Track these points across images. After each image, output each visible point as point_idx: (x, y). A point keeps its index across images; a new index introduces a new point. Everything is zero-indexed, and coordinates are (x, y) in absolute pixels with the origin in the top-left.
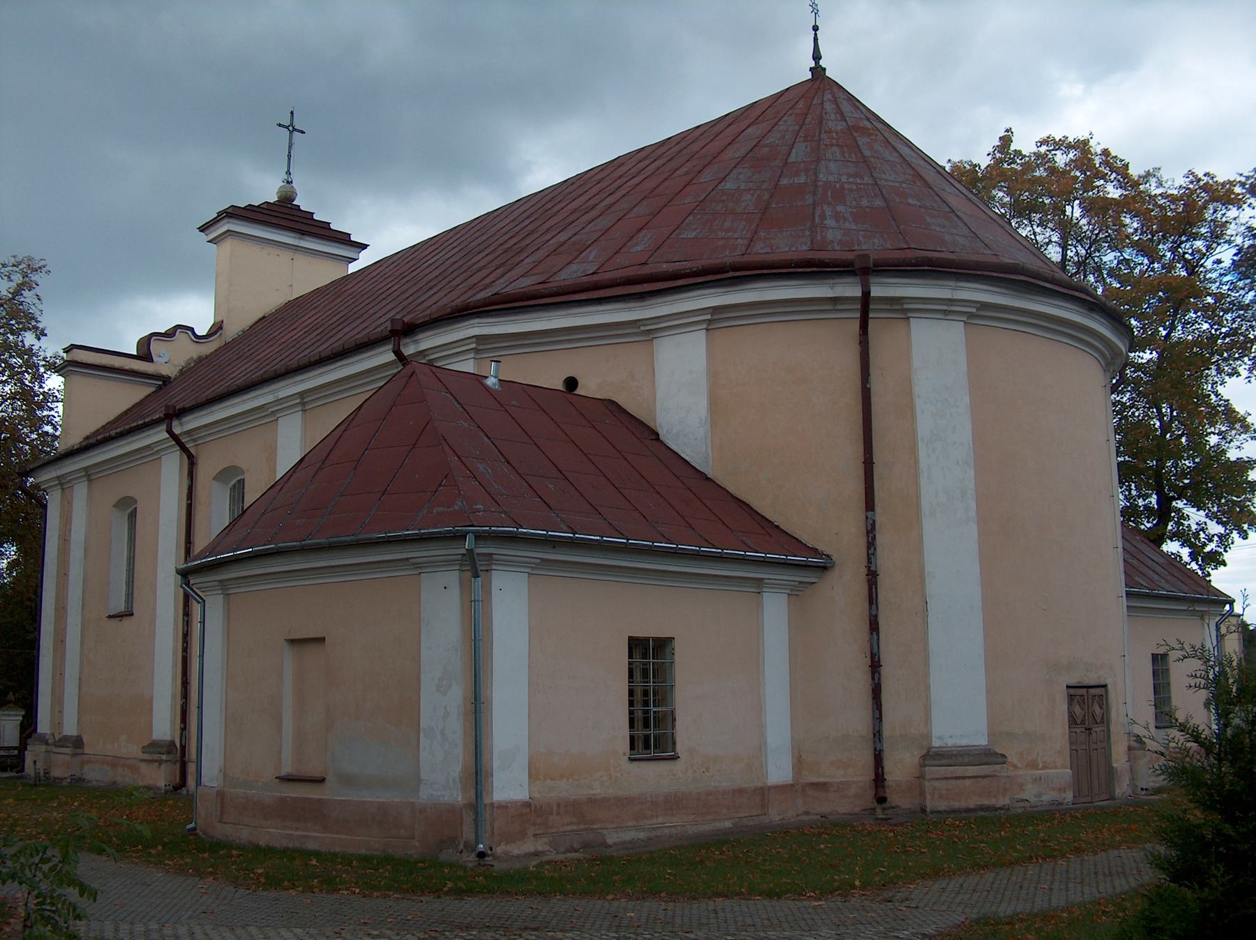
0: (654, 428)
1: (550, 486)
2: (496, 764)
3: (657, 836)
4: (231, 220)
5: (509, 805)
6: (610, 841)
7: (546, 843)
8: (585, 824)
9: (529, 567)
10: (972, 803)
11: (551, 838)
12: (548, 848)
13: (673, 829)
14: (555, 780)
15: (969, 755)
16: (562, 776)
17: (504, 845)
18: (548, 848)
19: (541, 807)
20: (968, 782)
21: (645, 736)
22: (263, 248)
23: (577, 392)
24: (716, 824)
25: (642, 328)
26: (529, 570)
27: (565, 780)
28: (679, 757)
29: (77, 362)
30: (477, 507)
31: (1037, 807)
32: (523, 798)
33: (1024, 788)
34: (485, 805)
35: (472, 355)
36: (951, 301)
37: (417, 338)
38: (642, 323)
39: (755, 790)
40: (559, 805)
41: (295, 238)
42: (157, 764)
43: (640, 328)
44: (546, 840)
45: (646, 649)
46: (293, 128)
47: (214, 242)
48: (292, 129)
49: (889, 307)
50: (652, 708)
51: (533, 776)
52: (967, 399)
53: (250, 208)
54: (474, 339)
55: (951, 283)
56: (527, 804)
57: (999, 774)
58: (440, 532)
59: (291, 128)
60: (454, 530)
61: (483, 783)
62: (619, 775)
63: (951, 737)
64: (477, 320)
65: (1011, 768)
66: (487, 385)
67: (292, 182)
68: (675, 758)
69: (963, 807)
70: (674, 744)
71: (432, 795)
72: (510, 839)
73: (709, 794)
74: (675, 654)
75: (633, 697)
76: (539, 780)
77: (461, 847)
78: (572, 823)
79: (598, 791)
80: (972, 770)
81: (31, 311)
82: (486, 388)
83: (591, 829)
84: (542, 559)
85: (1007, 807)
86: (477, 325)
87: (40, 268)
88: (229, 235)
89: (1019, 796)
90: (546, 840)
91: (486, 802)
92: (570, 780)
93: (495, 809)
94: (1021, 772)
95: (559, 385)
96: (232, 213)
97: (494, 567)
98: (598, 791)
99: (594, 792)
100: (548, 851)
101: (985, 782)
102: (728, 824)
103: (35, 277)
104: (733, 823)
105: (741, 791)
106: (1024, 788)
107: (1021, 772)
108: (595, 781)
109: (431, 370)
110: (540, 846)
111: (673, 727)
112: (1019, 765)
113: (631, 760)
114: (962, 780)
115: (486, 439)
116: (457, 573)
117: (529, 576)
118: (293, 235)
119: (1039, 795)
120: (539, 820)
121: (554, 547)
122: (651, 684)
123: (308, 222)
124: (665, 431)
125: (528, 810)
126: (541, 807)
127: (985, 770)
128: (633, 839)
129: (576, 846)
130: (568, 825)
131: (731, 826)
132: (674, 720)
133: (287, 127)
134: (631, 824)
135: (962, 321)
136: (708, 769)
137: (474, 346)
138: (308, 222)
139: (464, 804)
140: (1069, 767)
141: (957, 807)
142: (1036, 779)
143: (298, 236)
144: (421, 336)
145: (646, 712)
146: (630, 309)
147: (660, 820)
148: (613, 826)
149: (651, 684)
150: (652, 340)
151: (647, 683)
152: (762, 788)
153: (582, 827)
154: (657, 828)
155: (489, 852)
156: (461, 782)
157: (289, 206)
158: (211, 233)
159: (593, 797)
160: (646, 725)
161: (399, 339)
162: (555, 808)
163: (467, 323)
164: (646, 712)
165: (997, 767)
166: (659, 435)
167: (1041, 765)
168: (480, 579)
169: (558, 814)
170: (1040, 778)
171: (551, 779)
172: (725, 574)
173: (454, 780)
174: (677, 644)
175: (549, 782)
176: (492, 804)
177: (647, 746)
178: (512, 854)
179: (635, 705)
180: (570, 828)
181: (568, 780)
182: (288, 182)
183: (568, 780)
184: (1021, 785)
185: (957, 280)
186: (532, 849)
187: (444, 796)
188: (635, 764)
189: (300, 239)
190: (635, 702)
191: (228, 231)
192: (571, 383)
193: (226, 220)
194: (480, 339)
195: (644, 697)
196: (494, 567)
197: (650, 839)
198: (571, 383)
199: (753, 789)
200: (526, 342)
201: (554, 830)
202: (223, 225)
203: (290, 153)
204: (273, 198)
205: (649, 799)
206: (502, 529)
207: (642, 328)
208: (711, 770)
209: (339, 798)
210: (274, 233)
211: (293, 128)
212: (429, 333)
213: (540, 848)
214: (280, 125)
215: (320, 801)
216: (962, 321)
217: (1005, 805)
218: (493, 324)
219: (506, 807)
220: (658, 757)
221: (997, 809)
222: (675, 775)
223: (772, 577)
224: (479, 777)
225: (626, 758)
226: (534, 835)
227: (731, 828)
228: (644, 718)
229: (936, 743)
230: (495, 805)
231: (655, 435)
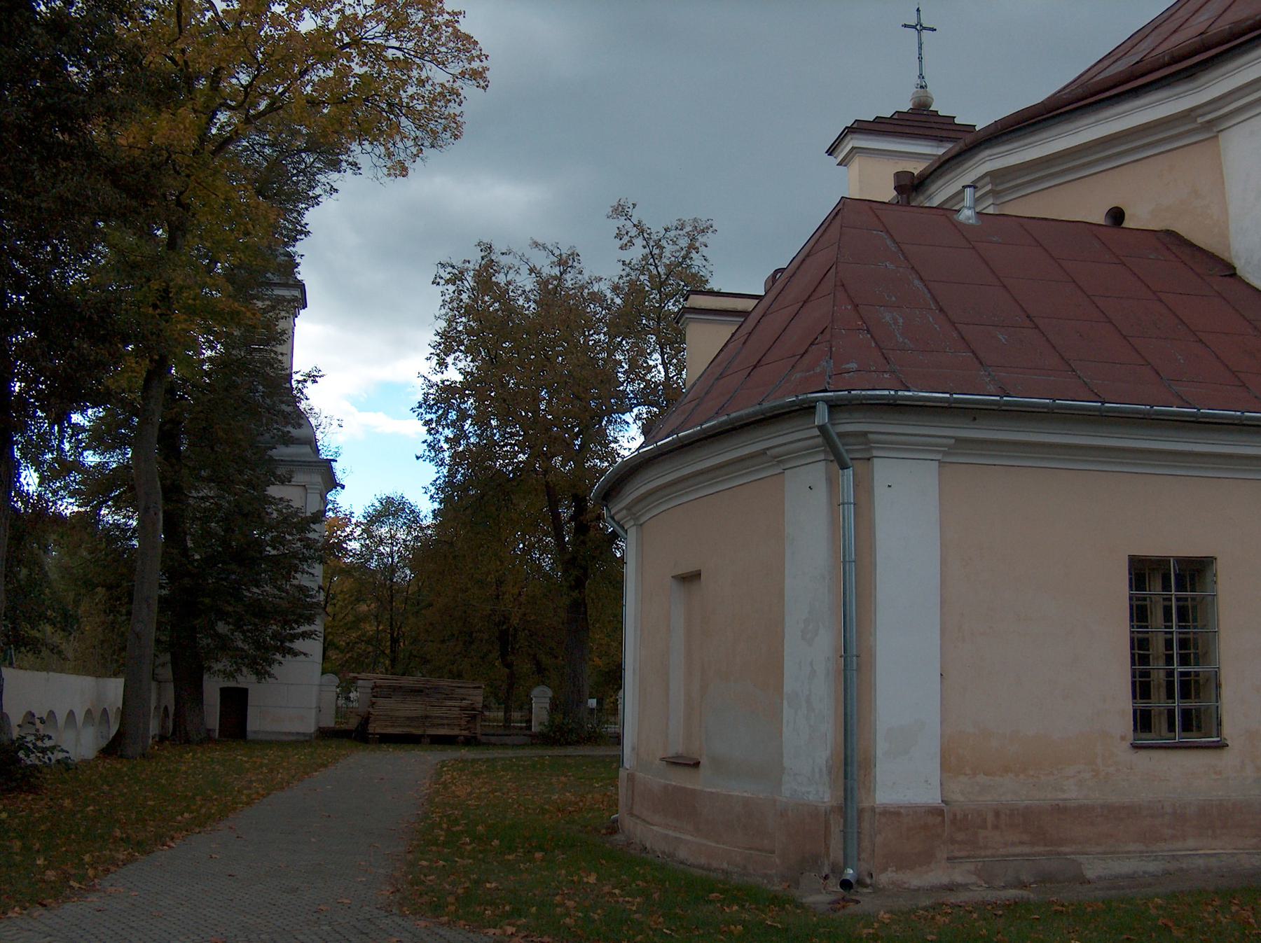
0: (1229, 261)
1: (1000, 337)
2: (881, 747)
3: (1181, 870)
4: (855, 136)
5: (902, 811)
6: (1090, 874)
8: (1046, 845)
9: (939, 452)
11: (980, 864)
12: (973, 879)
17: (892, 871)
18: (973, 879)
19: (966, 816)
22: (897, 163)
23: (1125, 225)
25: (1200, 120)
26: (939, 457)
28: (1228, 746)
29: (695, 309)
30: (848, 366)
32: (930, 801)
34: (861, 811)
35: (991, 201)
37: (929, 192)
38: (1200, 111)
40: (997, 814)
41: (932, 146)
42: (375, 728)
43: (1196, 121)
45: (1166, 579)
46: (921, 25)
47: (844, 164)
48: (919, 28)
50: (1175, 666)
51: (950, 764)
53: (879, 120)
54: (987, 179)
56: (936, 812)
59: (918, 27)
61: (855, 777)
64: (987, 152)
66: (960, 223)
67: (926, 86)
68: (1221, 746)
70: (1219, 724)
71: (796, 791)
74: (1219, 582)
75: (1166, 655)
76: (966, 774)
77: (826, 870)
78: (1022, 843)
79: (1072, 793)
81: (701, 273)
82: (959, 228)
83: (1059, 854)
84: (957, 439)
86: (987, 159)
87: (707, 228)
88: (856, 153)
90: (972, 867)
91: (866, 804)
92: (1022, 776)
93: (877, 816)
95: (1099, 217)
96: (858, 128)
97: (875, 453)
99: (1065, 796)
100: (973, 884)
103: (701, 239)
109: (871, 208)
111: (1218, 697)
113: (1136, 747)
115: (917, 282)
116: (822, 465)
117: (939, 467)
118: (930, 144)
120: (960, 836)
121: (975, 419)
123: (951, 127)
124: (1243, 261)
126: (966, 816)
128: (1135, 872)
129: (1025, 877)
130: (1013, 844)
132: (1218, 686)
133: (914, 27)
137: (989, 187)
138: (951, 127)
139: (832, 806)
143: (934, 143)
144: (933, 188)
145: (1170, 674)
146: (1178, 96)
147: (1191, 843)
150: (1216, 137)
153: (1037, 849)
155: (868, 881)
156: (830, 773)
157: (925, 113)
158: (839, 155)
159: (1061, 804)
160: (1185, 695)
161: (908, 198)
162: (990, 818)
163: (977, 159)
164: (1170, 674)
166: (1235, 268)
168: (850, 471)
169: (996, 827)
173: (821, 770)
174: (1221, 568)
176: (873, 809)
177: (1160, 724)
178: (906, 886)
179: (1151, 664)
180: (1018, 850)
182: (922, 87)
186: (945, 880)
187: (808, 793)
188: (1144, 754)
189: (938, 147)
190: (1151, 657)
191: (853, 148)
192: (1117, 216)
193: (849, 137)
194: (994, 175)
195: (1180, 650)
196: (875, 453)
197: (1167, 873)
198: (1117, 216)
200: (1053, 170)
201: (989, 852)
202: (847, 144)
203: (920, 54)
204: (906, 106)
206: (869, 392)
207: (1200, 120)
209: (709, 790)
210: (909, 144)
211: (921, 25)
212: (940, 183)
213: (959, 878)
214: (905, 26)
215: (693, 791)
218: (1009, 153)
219: (898, 814)
220: (1185, 745)
223: (891, 429)
224: (849, 768)
225: (1126, 744)
226: (948, 859)
228: (1167, 682)
230: (877, 810)
231: (1230, 271)
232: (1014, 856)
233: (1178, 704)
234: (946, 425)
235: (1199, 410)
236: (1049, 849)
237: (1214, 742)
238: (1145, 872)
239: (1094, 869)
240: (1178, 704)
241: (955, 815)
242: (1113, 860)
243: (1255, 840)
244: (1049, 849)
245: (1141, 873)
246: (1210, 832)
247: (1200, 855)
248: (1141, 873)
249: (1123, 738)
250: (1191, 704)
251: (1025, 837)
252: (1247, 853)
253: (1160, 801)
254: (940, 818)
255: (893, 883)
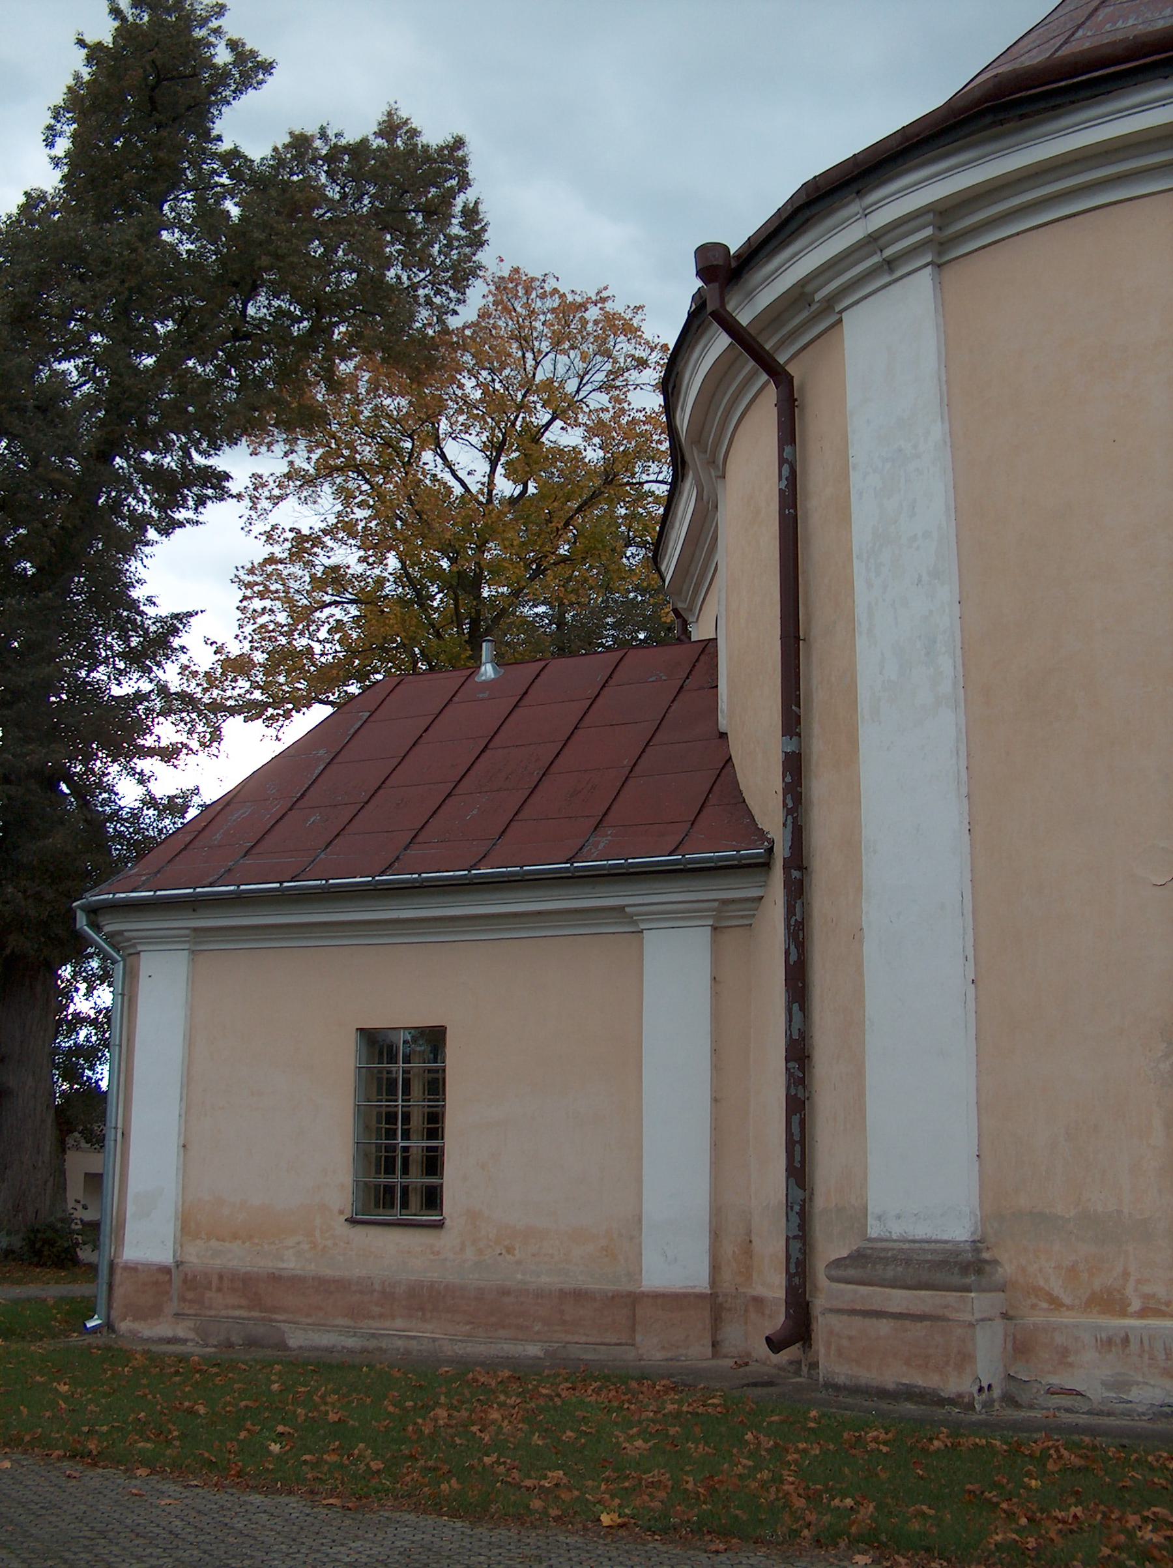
2: (131, 1209)
3: (380, 1349)
6: (292, 1343)
7: (190, 1329)
8: (261, 1312)
9: (185, 942)
10: (892, 1375)
11: (199, 1322)
12: (191, 1335)
13: (414, 1342)
14: (224, 1240)
15: (908, 1262)
16: (235, 1237)
18: (191, 1335)
19: (195, 1277)
20: (884, 1327)
21: (375, 1185)
24: (505, 1346)
27: (239, 1242)
31: (1110, 1414)
33: (1070, 1360)
36: (873, 241)
39: (613, 1297)
40: (221, 1277)
44: (190, 1324)
49: (805, 314)
52: (938, 431)
55: (855, 208)
56: (165, 1270)
57: (954, 1315)
58: (710, 859)
60: (683, 860)
62: (329, 1243)
63: (898, 1217)
65: (1045, 1305)
69: (875, 1384)
72: (141, 1314)
73: (505, 1292)
76: (201, 1238)
78: (240, 1307)
79: (291, 1264)
80: (898, 1299)
83: (271, 1320)
84: (195, 929)
85: (966, 1400)
89: (1055, 1380)
92: (248, 1244)
94: (1067, 1318)
98: (292, 1265)
99: (285, 1265)
101: (918, 1330)
102: (534, 1350)
104: (547, 1352)
105: (579, 1296)
106: (1070, 1360)
107: (1067, 1318)
108: (288, 1248)
110: (182, 1330)
112: (1067, 1301)
113: (352, 1221)
114: (874, 1320)
119: (1120, 1385)
120: (190, 1295)
122: (400, 1102)
125: (168, 1277)
127: (923, 1301)
128: (334, 1346)
130: (234, 1307)
131: (541, 1354)
134: (340, 1321)
135: (927, 265)
136: (510, 1250)
140: (119, 1271)
141: (863, 1381)
142: (1110, 1342)
148: (309, 1321)
149: (400, 1102)
151: (438, 1100)
152: (630, 1294)
154: (381, 1335)
165: (951, 1297)
167: (1136, 1305)
169: (219, 1290)
170: (1126, 1341)
171: (218, 1240)
172: (350, 918)
175: (214, 1243)
178: (140, 1335)
180: (237, 1313)
181: (244, 1243)
183: (244, 1243)
184: (1064, 1352)
185: (860, 194)
186: (170, 1334)
188: (360, 1230)
196: (140, 948)
197: (364, 1350)
199: (610, 1294)
201: (213, 1313)
205: (377, 1287)
208: (517, 1252)
213: (181, 1334)
216: (927, 265)
217: (960, 1396)
220: (408, 1222)
221: (942, 1402)
222: (438, 1253)
223: (647, 900)
227: (540, 1358)
229: (874, 1230)
232: (232, 1318)
233: (398, 1180)
234: (630, 893)
235: (683, 856)
236: (263, 1315)
237: (435, 1220)
238: (343, 1347)
239: (296, 1339)
240: (398, 1180)
241: (186, 1275)
242: (313, 1331)
243: (468, 1327)
244: (263, 1315)
245: (340, 1348)
246: (420, 1314)
247: (400, 1337)
248: (340, 1348)
249: (341, 1212)
250: (383, 1180)
251: (244, 1302)
252: (450, 1340)
253: (369, 1278)
254: (168, 1277)
255: (130, 1331)
